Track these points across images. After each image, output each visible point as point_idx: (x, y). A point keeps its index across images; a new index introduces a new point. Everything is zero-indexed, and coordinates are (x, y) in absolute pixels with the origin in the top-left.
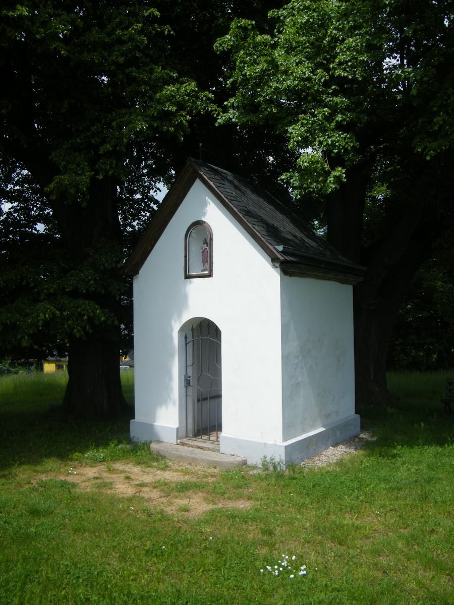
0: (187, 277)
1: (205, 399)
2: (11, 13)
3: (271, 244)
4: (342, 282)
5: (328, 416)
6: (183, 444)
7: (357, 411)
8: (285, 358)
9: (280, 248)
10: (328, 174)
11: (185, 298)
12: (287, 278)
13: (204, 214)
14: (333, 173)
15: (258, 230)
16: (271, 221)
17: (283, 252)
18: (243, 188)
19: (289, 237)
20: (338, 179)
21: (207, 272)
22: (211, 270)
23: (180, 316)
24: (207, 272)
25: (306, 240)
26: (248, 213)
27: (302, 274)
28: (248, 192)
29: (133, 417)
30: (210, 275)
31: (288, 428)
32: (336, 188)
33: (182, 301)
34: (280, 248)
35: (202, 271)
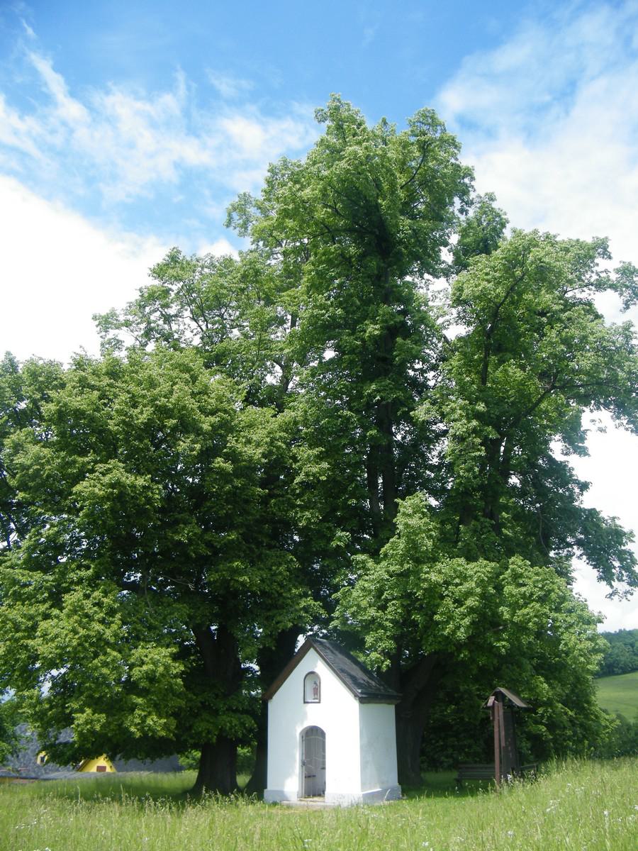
0: (305, 702)
1: (309, 777)
2: (129, 479)
3: (501, 762)
4: (389, 704)
5: (383, 783)
6: (301, 800)
7: (400, 782)
8: (362, 747)
9: (360, 691)
10: (383, 662)
11: (305, 714)
12: (362, 705)
13: (316, 666)
14: (385, 663)
15: (348, 680)
16: (353, 673)
17: (361, 693)
18: (335, 652)
19: (362, 682)
20: (387, 666)
21: (317, 701)
22: (320, 700)
23: (302, 723)
24: (317, 701)
25: (370, 681)
26: (343, 671)
27: (369, 702)
28: (337, 653)
29: (266, 788)
30: (319, 702)
31: (363, 785)
32: (402, 276)
33: (304, 716)
34: (360, 691)
35: (314, 699)
